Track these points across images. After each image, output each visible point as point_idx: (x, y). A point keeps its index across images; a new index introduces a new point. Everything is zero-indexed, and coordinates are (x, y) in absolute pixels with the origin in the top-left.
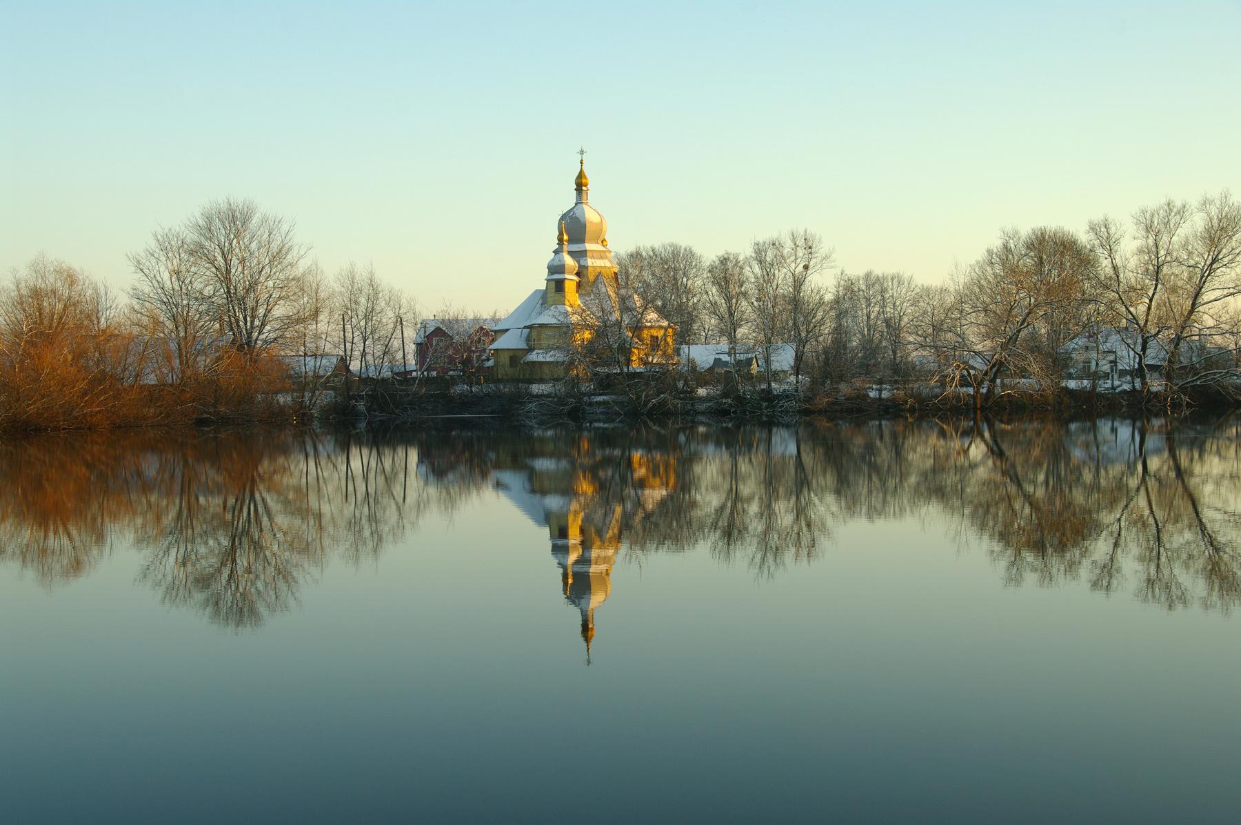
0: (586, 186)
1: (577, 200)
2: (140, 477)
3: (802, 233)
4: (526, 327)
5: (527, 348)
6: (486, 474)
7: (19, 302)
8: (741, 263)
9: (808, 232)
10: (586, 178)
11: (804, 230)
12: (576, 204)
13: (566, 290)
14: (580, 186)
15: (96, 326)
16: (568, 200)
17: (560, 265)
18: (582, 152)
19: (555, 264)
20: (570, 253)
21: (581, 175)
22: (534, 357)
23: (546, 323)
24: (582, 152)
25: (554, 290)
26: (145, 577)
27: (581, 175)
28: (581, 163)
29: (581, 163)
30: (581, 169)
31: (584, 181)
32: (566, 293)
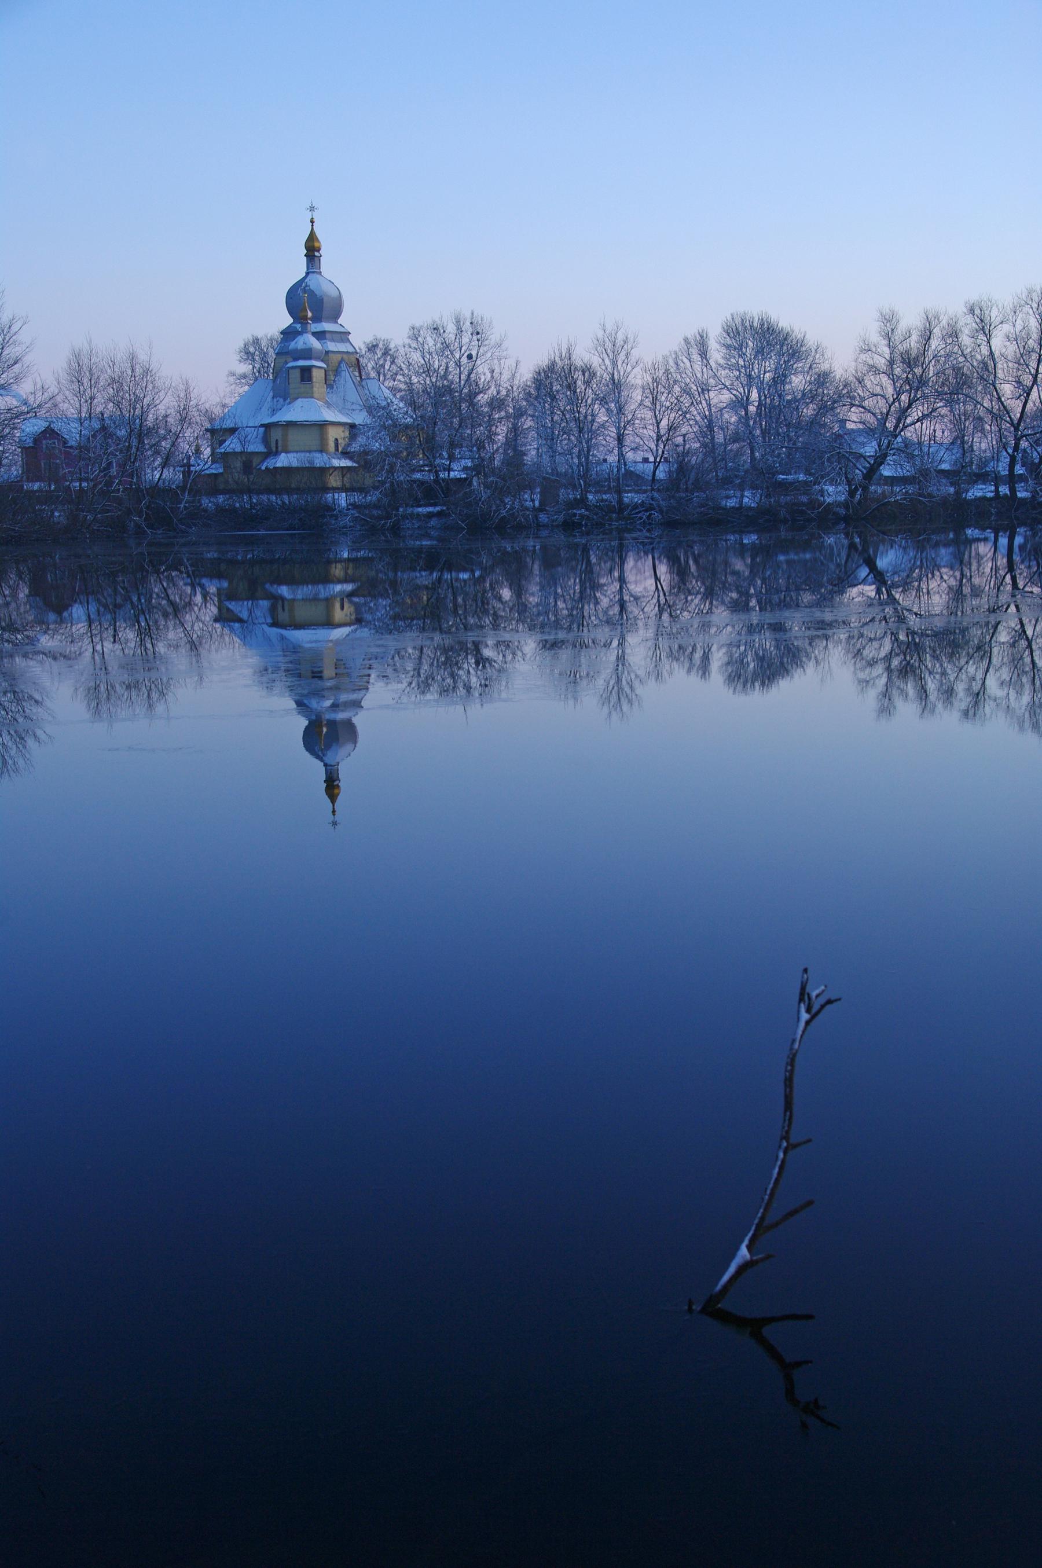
0: (319, 250)
1: (307, 270)
2: (755, 652)
3: (468, 315)
4: (262, 426)
5: (265, 450)
6: (736, 611)
7: (414, 345)
8: (393, 350)
9: (475, 314)
10: (318, 241)
11: (470, 312)
12: (307, 274)
13: (314, 380)
14: (312, 250)
15: (762, 376)
16: (299, 268)
17: (305, 349)
18: (312, 209)
19: (299, 348)
20: (314, 334)
21: (312, 238)
22: (283, 460)
23: (294, 420)
24: (312, 209)
25: (299, 379)
26: (110, 750)
27: (312, 238)
28: (312, 222)
29: (312, 222)
30: (312, 229)
31: (316, 244)
32: (314, 384)
